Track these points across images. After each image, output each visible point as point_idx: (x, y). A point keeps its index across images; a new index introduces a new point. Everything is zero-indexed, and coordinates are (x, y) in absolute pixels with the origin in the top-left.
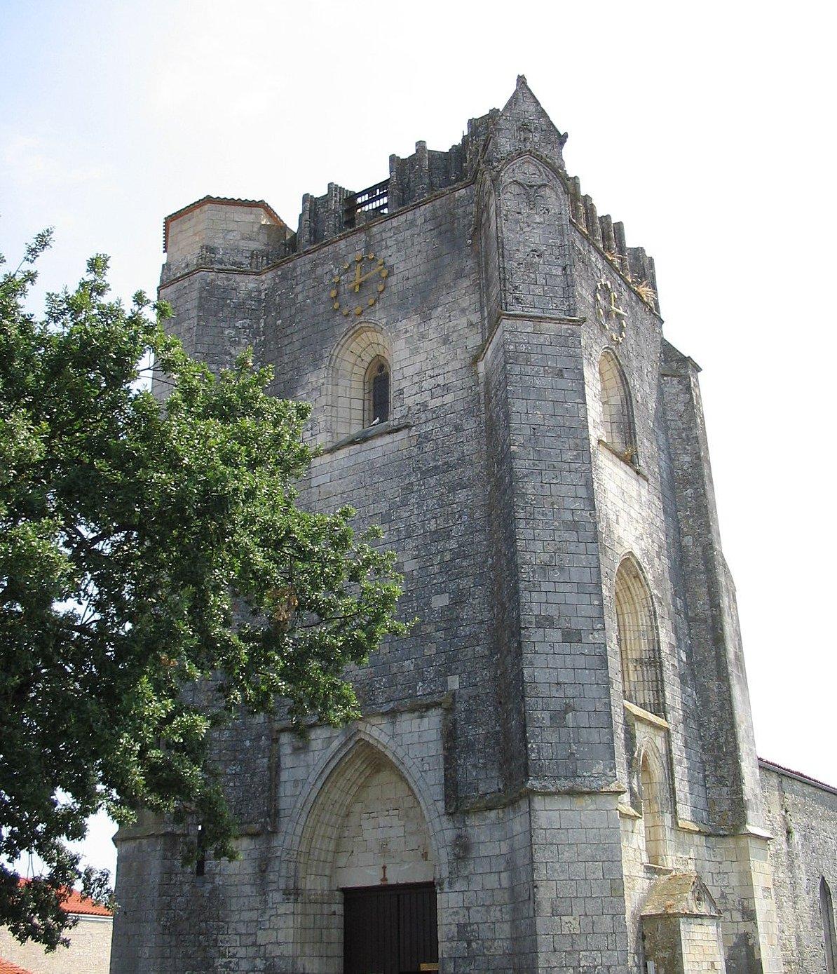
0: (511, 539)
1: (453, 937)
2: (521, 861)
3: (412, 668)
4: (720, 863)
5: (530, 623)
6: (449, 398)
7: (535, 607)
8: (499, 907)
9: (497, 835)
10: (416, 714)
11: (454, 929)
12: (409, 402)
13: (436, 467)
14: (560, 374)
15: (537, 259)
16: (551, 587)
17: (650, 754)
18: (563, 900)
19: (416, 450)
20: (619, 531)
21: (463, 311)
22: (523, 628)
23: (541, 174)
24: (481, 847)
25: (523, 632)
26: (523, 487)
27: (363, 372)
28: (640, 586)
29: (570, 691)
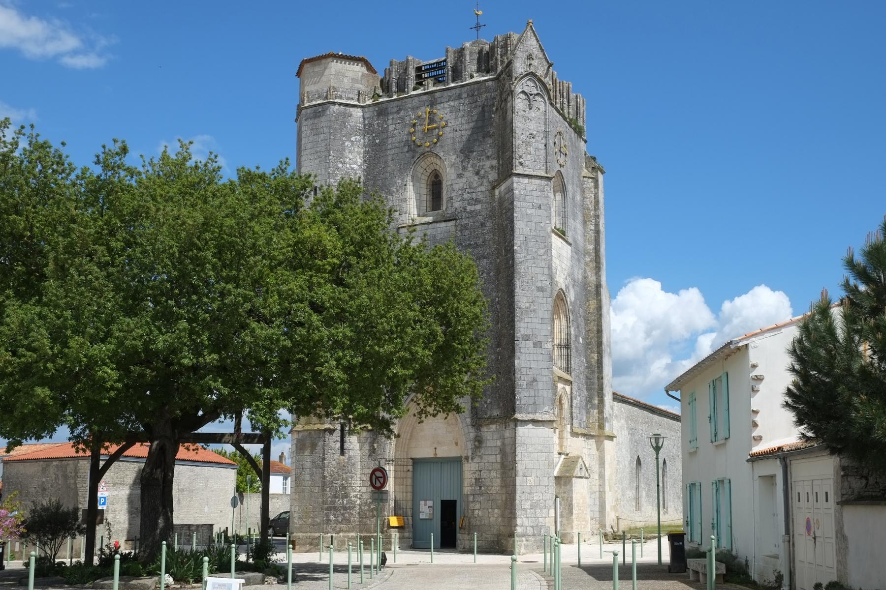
0: (511, 293)
2: (508, 450)
6: (478, 207)
14: (540, 207)
17: (563, 395)
29: (536, 372)
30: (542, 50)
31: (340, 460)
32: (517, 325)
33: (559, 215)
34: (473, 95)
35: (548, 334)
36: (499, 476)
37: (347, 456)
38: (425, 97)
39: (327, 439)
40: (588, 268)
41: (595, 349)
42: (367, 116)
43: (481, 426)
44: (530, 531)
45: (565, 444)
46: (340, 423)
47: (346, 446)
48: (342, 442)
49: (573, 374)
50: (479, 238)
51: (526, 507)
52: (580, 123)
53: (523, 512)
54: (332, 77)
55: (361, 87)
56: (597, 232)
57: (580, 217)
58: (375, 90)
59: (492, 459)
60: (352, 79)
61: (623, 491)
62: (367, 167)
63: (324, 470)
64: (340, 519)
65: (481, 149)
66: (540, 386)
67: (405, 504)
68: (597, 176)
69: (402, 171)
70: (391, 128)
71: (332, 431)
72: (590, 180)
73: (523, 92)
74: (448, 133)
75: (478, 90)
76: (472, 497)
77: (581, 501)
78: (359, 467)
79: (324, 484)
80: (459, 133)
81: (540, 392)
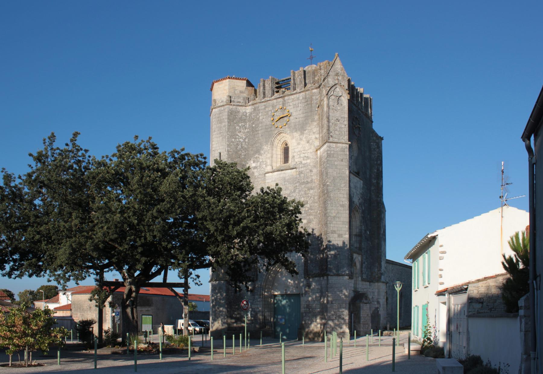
6: (308, 161)
11: (306, 306)
12: (296, 160)
15: (338, 122)
21: (314, 133)
70: (261, 118)
80: (298, 120)
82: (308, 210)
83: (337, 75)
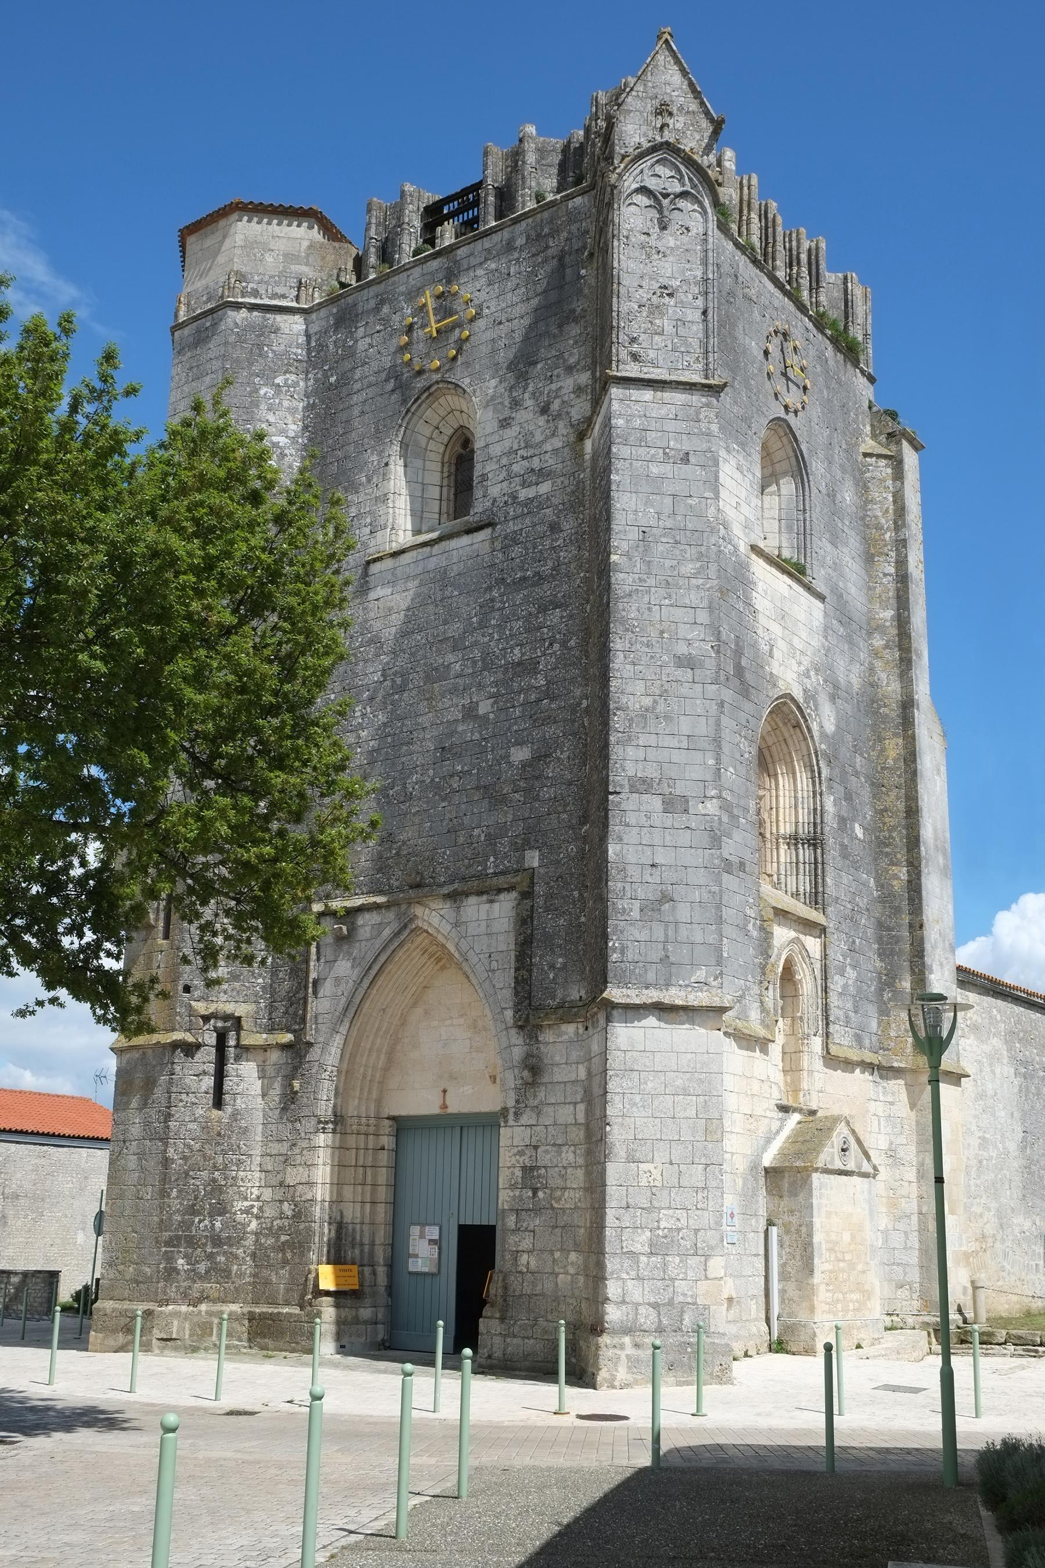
0: (604, 678)
1: (516, 1183)
2: (597, 1091)
3: (483, 839)
4: (892, 1103)
5: (622, 786)
6: (545, 488)
7: (629, 765)
8: (572, 1148)
9: (574, 1056)
10: (485, 897)
11: (518, 1173)
13: (524, 579)
14: (686, 459)
16: (652, 740)
17: (798, 959)
18: (643, 1142)
19: (500, 555)
20: (775, 667)
22: (612, 793)
23: (682, 176)
24: (555, 1069)
25: (611, 797)
26: (624, 610)
27: (442, 449)
28: (802, 738)
29: (670, 876)
30: (696, 94)
31: (208, 1120)
32: (616, 752)
33: (789, 529)
34: (539, 236)
35: (709, 777)
36: (581, 1161)
37: (229, 1109)
38: (434, 264)
39: (177, 1068)
40: (878, 664)
41: (902, 856)
42: (314, 329)
43: (540, 1027)
44: (647, 1318)
45: (805, 1085)
46: (216, 1029)
47: (228, 1084)
48: (220, 1076)
49: (830, 910)
50: (545, 560)
51: (637, 1248)
52: (857, 333)
53: (627, 1263)
54: (238, 251)
55: (307, 271)
56: (903, 578)
57: (853, 542)
58: (338, 276)
59: (565, 1114)
60: (286, 255)
61: (1000, 1214)
62: (310, 440)
63: (166, 1145)
64: (202, 1268)
65: (554, 353)
66: (683, 912)
67: (367, 1234)
68: (900, 451)
69: (379, 436)
70: (362, 345)
71: (190, 1049)
72: (883, 462)
73: (643, 190)
74: (482, 332)
75: (551, 221)
76: (513, 1218)
77: (846, 1237)
78: (259, 1138)
79: (164, 1179)
80: (504, 328)
81: (684, 932)
82: (539, 700)
83: (663, 110)
